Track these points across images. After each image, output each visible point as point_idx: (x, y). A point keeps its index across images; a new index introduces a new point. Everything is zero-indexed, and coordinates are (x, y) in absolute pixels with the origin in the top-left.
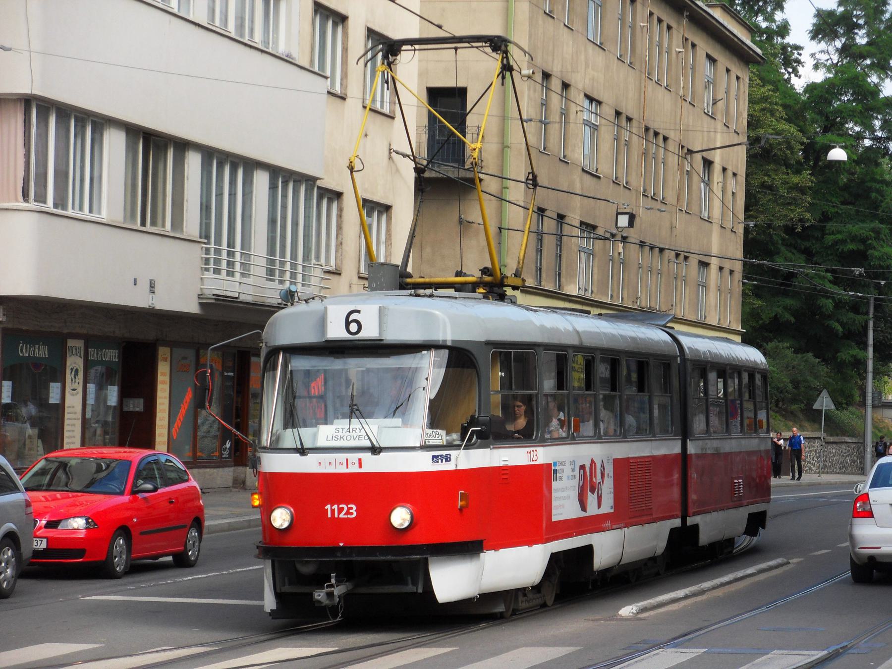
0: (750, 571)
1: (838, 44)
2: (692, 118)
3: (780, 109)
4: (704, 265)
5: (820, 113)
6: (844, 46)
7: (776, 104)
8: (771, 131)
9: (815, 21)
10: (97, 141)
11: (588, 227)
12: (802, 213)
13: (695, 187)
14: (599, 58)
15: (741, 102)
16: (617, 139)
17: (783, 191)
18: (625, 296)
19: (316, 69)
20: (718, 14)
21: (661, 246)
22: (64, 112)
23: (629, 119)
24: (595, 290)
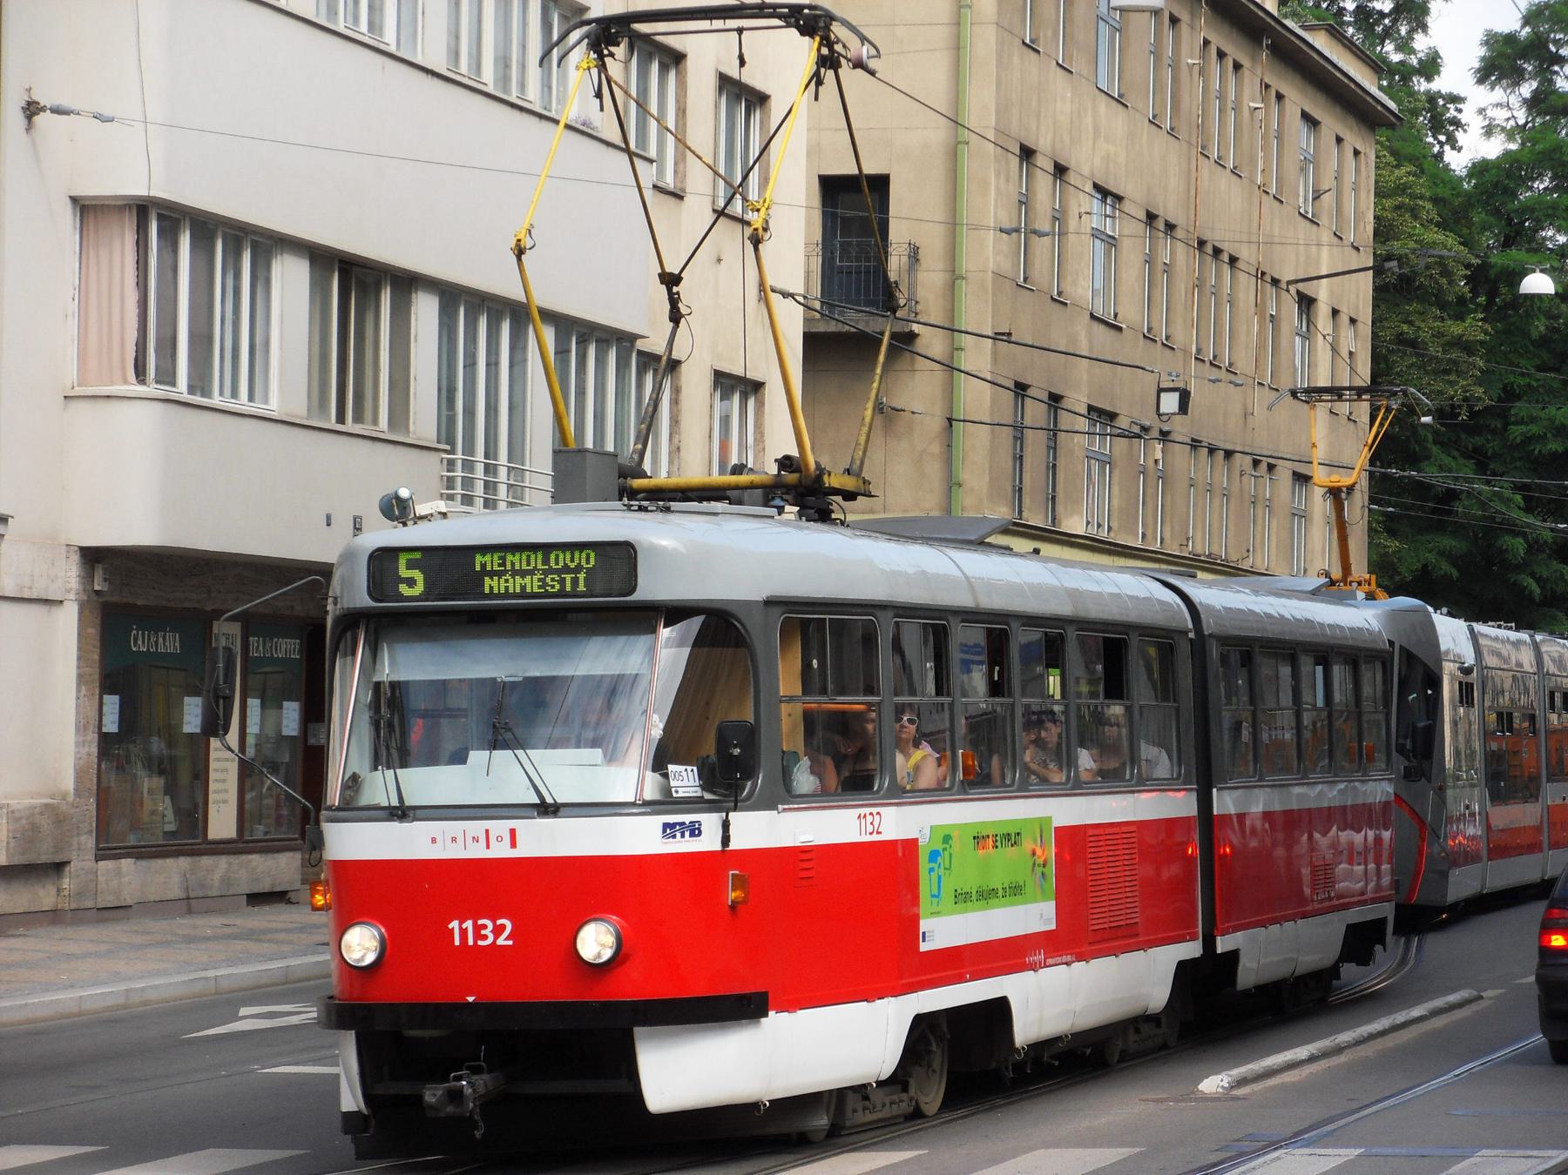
0: (1416, 1012)
1: (1527, 89)
2: (1277, 222)
3: (1429, 205)
5: (1497, 212)
6: (1536, 93)
7: (1422, 197)
8: (1412, 245)
9: (1482, 51)
10: (261, 277)
11: (1102, 416)
13: (1284, 343)
14: (1116, 121)
15: (1363, 195)
16: (1150, 261)
17: (1434, 350)
18: (1167, 535)
20: (1321, 41)
21: (1229, 447)
22: (206, 227)
23: (1170, 227)
24: (1114, 524)
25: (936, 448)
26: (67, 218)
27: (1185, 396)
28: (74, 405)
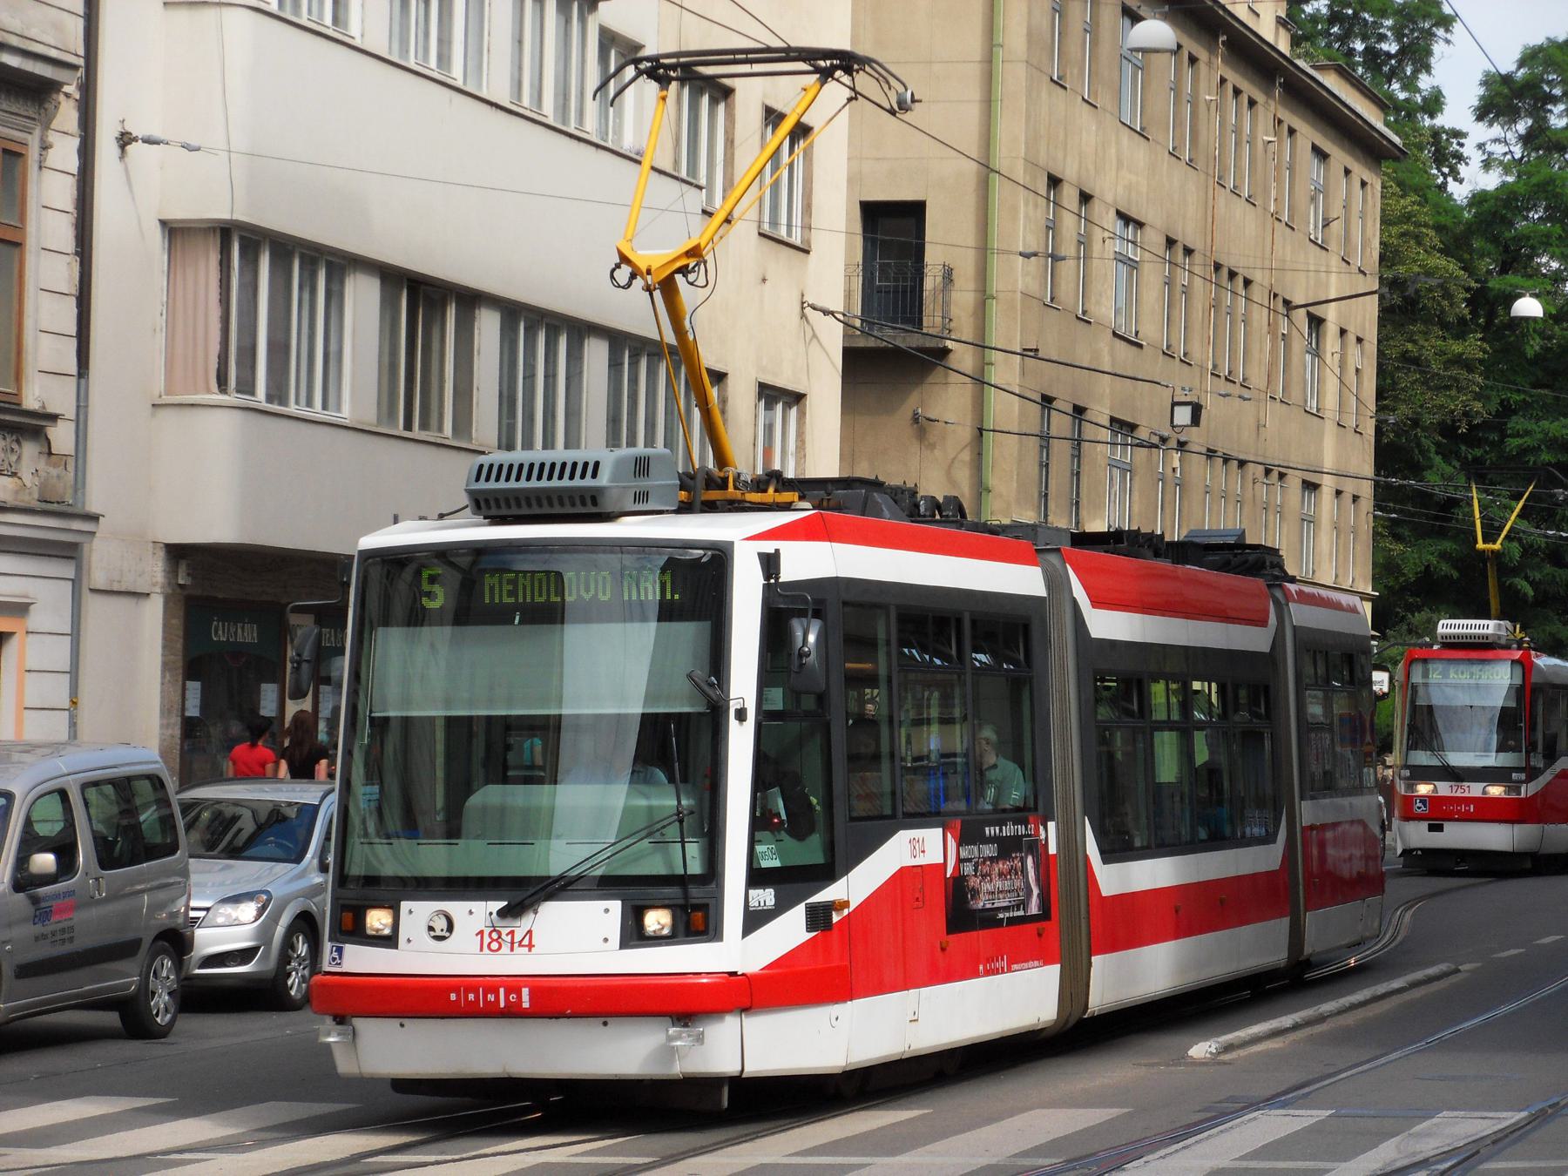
3: (1432, 233)
4: (1311, 487)
7: (1426, 225)
11: (1122, 426)
12: (1468, 402)
19: (683, 174)
20: (1331, 81)
21: (1242, 457)
23: (1188, 252)
25: (966, 456)
26: (156, 237)
27: (1197, 410)
28: (162, 413)
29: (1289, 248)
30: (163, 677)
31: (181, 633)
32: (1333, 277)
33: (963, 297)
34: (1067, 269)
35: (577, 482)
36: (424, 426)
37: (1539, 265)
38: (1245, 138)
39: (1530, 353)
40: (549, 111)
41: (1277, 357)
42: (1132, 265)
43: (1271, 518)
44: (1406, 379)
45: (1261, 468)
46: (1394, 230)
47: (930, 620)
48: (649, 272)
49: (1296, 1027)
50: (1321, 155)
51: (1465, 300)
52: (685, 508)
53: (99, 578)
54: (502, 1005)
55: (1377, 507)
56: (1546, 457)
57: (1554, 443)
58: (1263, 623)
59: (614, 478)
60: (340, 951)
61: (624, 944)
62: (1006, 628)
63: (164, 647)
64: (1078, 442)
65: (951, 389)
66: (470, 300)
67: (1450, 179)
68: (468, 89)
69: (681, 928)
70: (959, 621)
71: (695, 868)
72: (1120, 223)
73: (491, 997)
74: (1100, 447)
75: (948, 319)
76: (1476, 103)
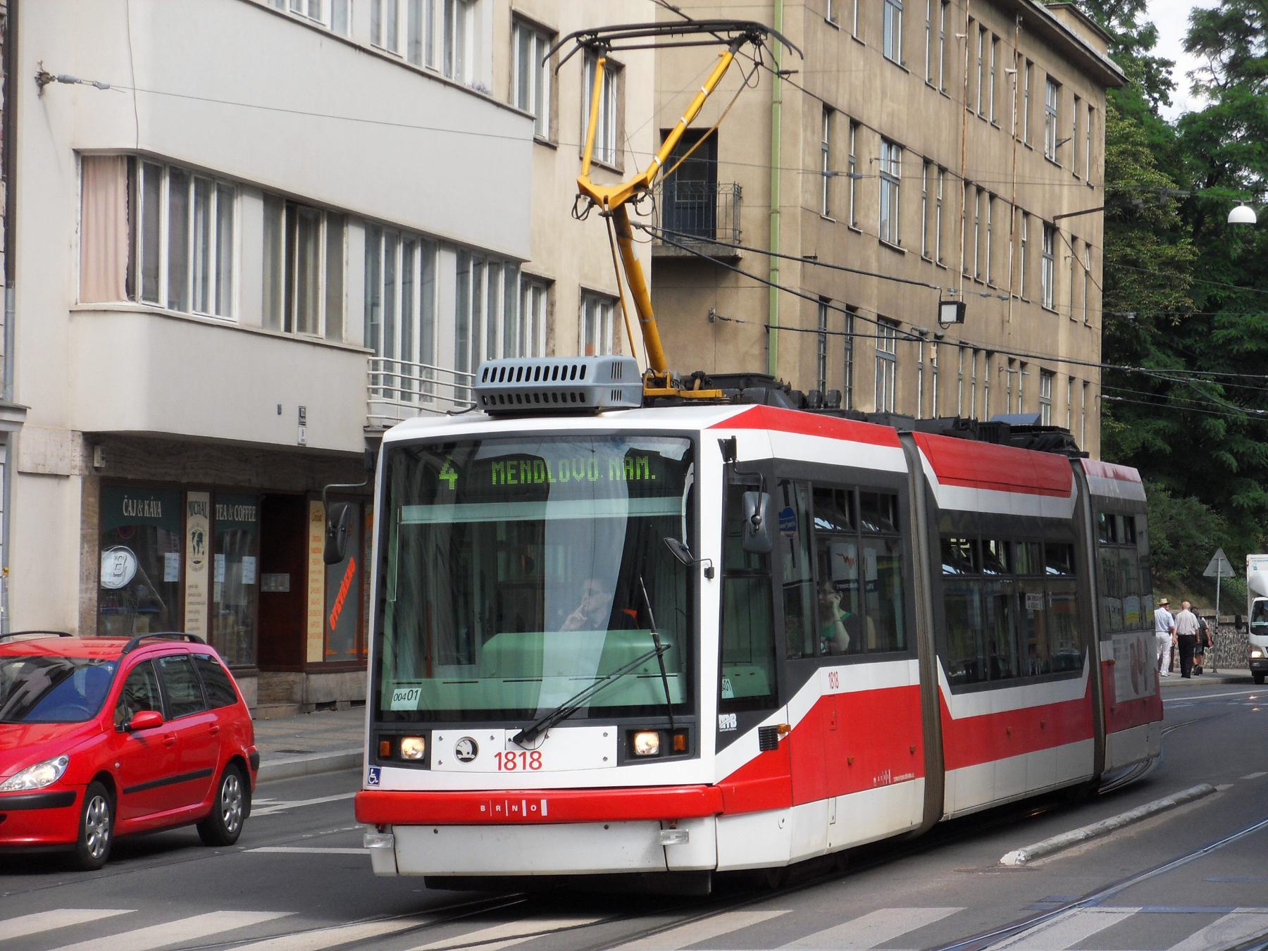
3: (1147, 151)
4: (1048, 374)
7: (1142, 144)
11: (888, 323)
12: (1180, 299)
19: (516, 106)
20: (1062, 18)
21: (989, 348)
23: (942, 170)
27: (961, 308)
28: (82, 320)
29: (1028, 166)
30: (82, 548)
31: (97, 510)
32: (1066, 190)
33: (752, 212)
34: (841, 183)
35: (568, 382)
36: (302, 328)
37: (1241, 178)
38: (990, 70)
39: (1234, 255)
40: (403, 52)
41: (1018, 260)
42: (895, 182)
43: (1014, 402)
44: (1127, 279)
45: (1005, 358)
46: (1114, 149)
47: (835, 492)
48: (606, 201)
49: (1088, 838)
50: (1054, 84)
51: (1177, 208)
52: (648, 402)
53: (26, 463)
54: (525, 814)
55: (1104, 391)
56: (1250, 346)
57: (1254, 334)
58: (1065, 493)
59: (598, 379)
60: (377, 773)
61: (621, 762)
62: (876, 500)
63: (83, 522)
64: (850, 337)
65: (742, 291)
66: (340, 218)
67: (1160, 103)
68: (335, 33)
69: (666, 747)
70: (851, 494)
71: (676, 697)
72: (884, 146)
73: (515, 808)
74: (869, 341)
75: (737, 230)
76: (1186, 36)
